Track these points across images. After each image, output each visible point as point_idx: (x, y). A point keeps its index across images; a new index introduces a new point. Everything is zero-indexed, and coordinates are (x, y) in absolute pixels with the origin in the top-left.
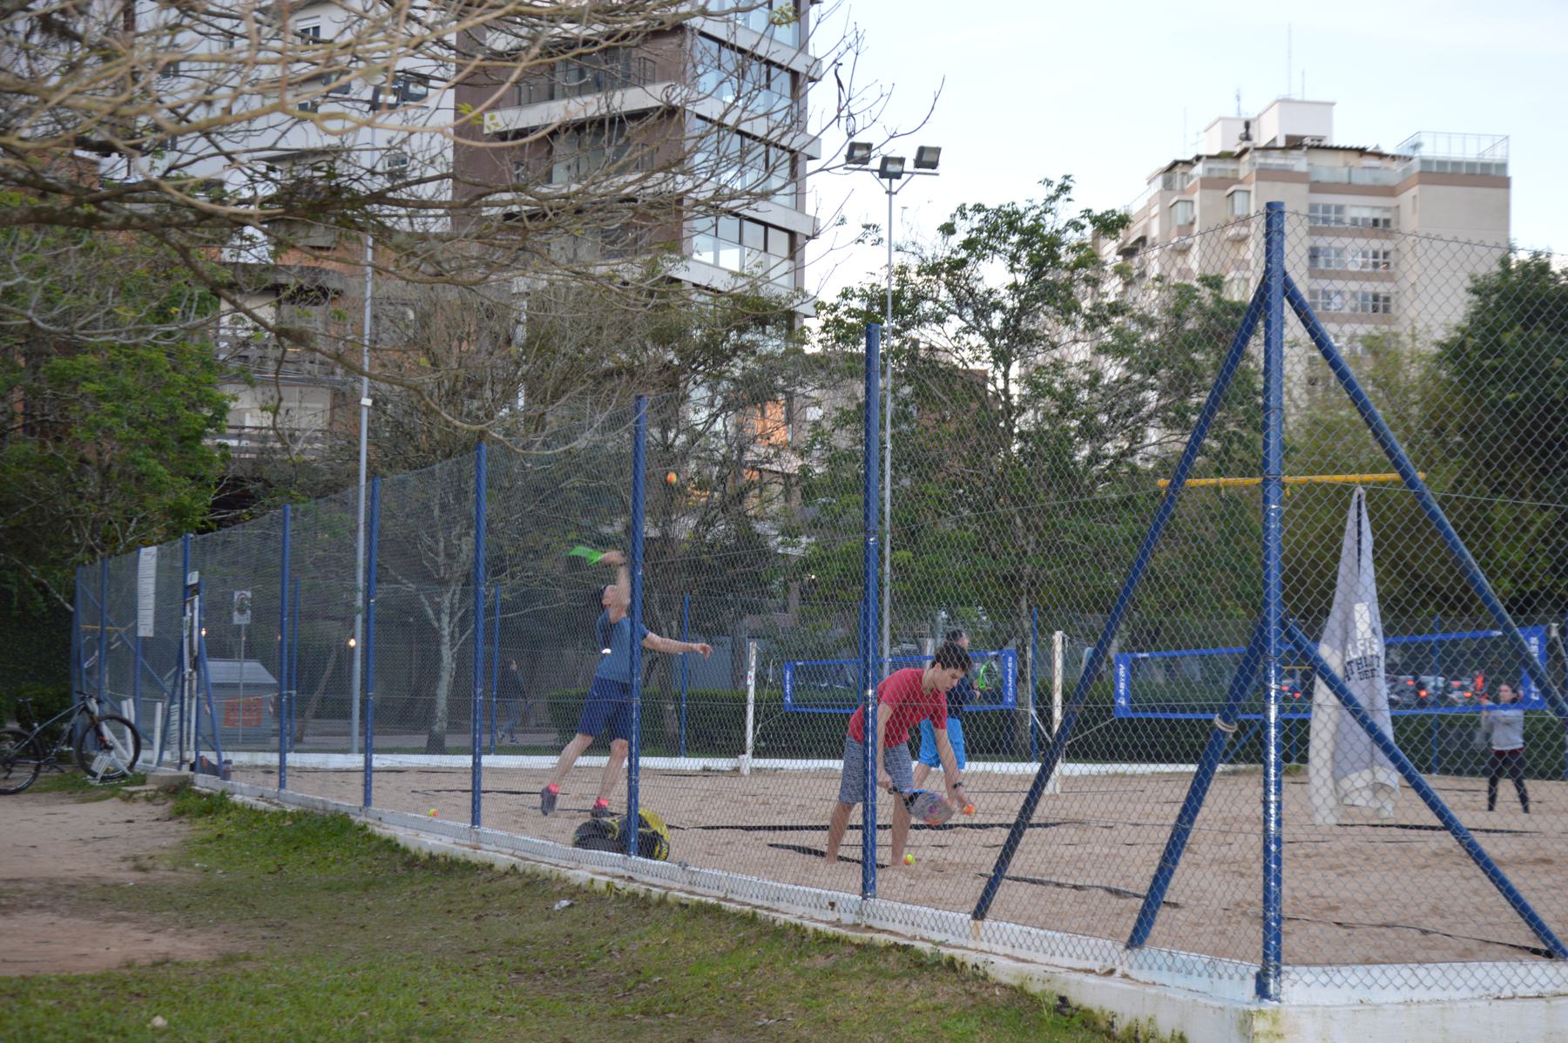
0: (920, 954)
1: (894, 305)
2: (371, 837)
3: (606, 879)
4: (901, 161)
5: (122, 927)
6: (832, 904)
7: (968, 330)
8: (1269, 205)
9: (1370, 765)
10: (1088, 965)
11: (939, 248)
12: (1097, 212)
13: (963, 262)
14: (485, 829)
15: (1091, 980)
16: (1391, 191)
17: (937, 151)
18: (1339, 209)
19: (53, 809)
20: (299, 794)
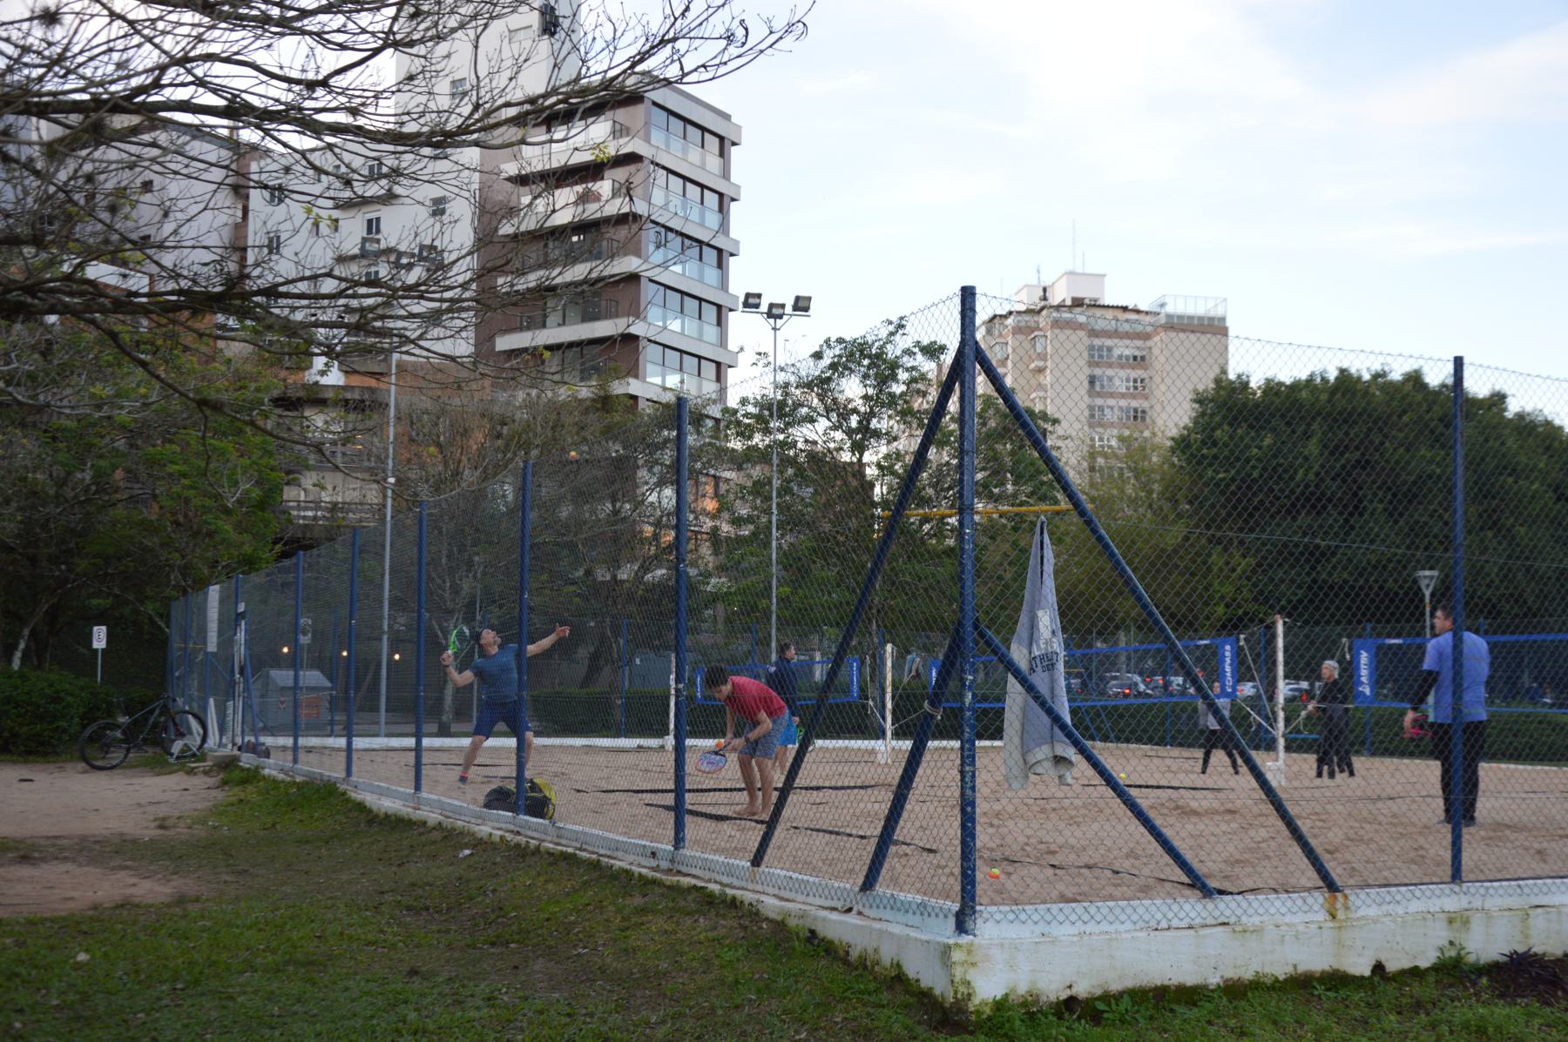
0: (711, 895)
1: (778, 410)
2: (348, 800)
3: (500, 833)
4: (783, 306)
5: (123, 873)
6: (654, 854)
7: (835, 428)
8: (964, 289)
9: (1052, 741)
10: (833, 904)
11: (811, 369)
12: (925, 342)
13: (829, 379)
14: (424, 795)
15: (834, 916)
16: (1146, 337)
17: (809, 299)
18: (1110, 349)
19: (134, 781)
20: (310, 766)
